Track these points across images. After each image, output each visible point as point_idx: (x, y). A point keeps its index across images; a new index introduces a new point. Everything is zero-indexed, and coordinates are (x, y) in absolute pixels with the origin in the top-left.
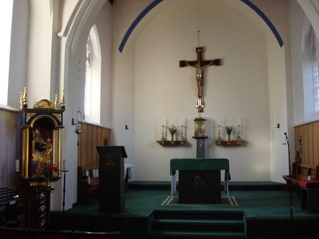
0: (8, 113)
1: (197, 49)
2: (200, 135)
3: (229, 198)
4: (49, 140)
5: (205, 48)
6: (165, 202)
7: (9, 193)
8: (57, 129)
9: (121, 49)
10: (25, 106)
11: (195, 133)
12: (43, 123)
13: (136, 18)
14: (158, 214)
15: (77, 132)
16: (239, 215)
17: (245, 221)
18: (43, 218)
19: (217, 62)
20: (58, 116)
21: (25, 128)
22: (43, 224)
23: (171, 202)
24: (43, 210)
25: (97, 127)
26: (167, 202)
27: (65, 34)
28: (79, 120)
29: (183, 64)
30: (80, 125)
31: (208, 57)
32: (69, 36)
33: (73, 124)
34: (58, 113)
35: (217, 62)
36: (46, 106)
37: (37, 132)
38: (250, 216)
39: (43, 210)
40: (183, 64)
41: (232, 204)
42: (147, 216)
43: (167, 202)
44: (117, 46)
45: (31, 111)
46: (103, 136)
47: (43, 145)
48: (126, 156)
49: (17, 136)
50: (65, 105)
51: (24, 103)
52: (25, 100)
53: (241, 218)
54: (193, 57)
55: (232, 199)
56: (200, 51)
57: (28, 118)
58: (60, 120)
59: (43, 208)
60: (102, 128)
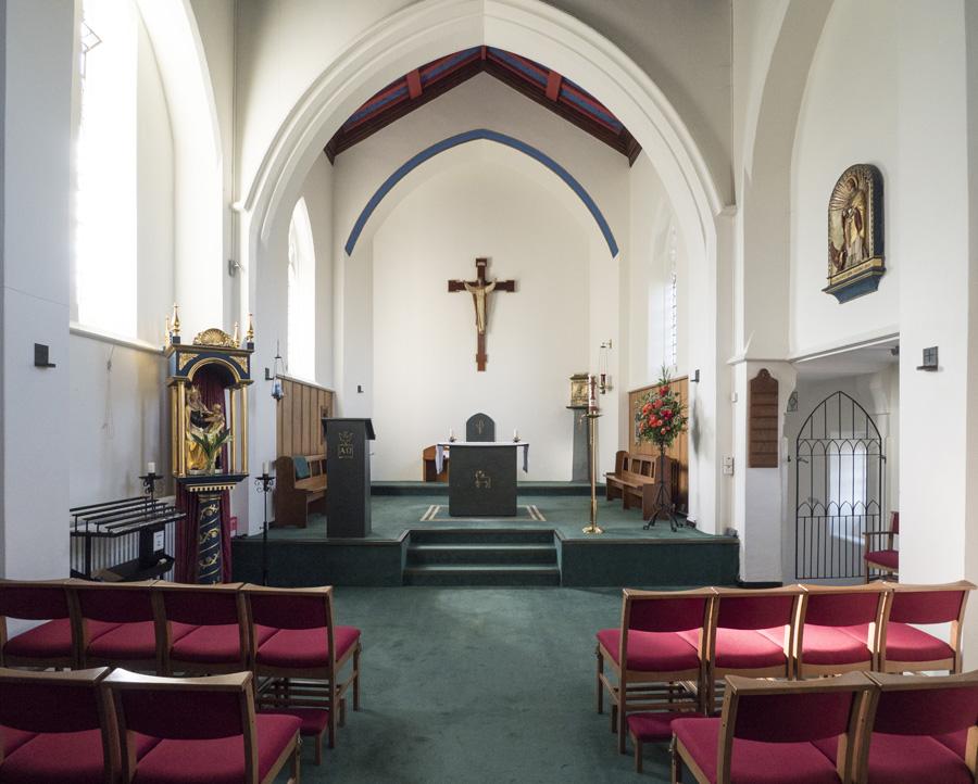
0: (140, 354)
1: (478, 260)
2: (581, 403)
3: (528, 507)
4: (219, 406)
5: (491, 259)
6: (426, 516)
7: (160, 510)
8: (239, 387)
9: (349, 248)
10: (176, 340)
11: (572, 401)
12: (213, 373)
13: (380, 186)
14: (417, 536)
15: (276, 396)
16: (548, 536)
17: (558, 546)
18: (215, 550)
19: (509, 286)
20: (241, 361)
21: (175, 384)
22: (214, 561)
23: (438, 515)
24: (214, 535)
25: (310, 387)
26: (430, 515)
27: (248, 206)
28: (280, 373)
29: (455, 286)
30: (280, 381)
31: (497, 273)
32: (256, 209)
33: (267, 379)
34: (240, 356)
35: (509, 286)
36: (216, 341)
37: (194, 390)
38: (568, 538)
39: (214, 535)
40: (455, 286)
41: (533, 516)
42: (400, 540)
43: (430, 515)
44: (347, 241)
45: (186, 349)
46: (321, 403)
47: (206, 416)
48: (372, 437)
49: (161, 398)
50: (253, 340)
51: (174, 335)
52: (174, 328)
53: (551, 541)
54: (472, 276)
55: (532, 509)
56: (482, 266)
57: (183, 363)
58: (246, 370)
59: (214, 532)
60: (318, 389)
